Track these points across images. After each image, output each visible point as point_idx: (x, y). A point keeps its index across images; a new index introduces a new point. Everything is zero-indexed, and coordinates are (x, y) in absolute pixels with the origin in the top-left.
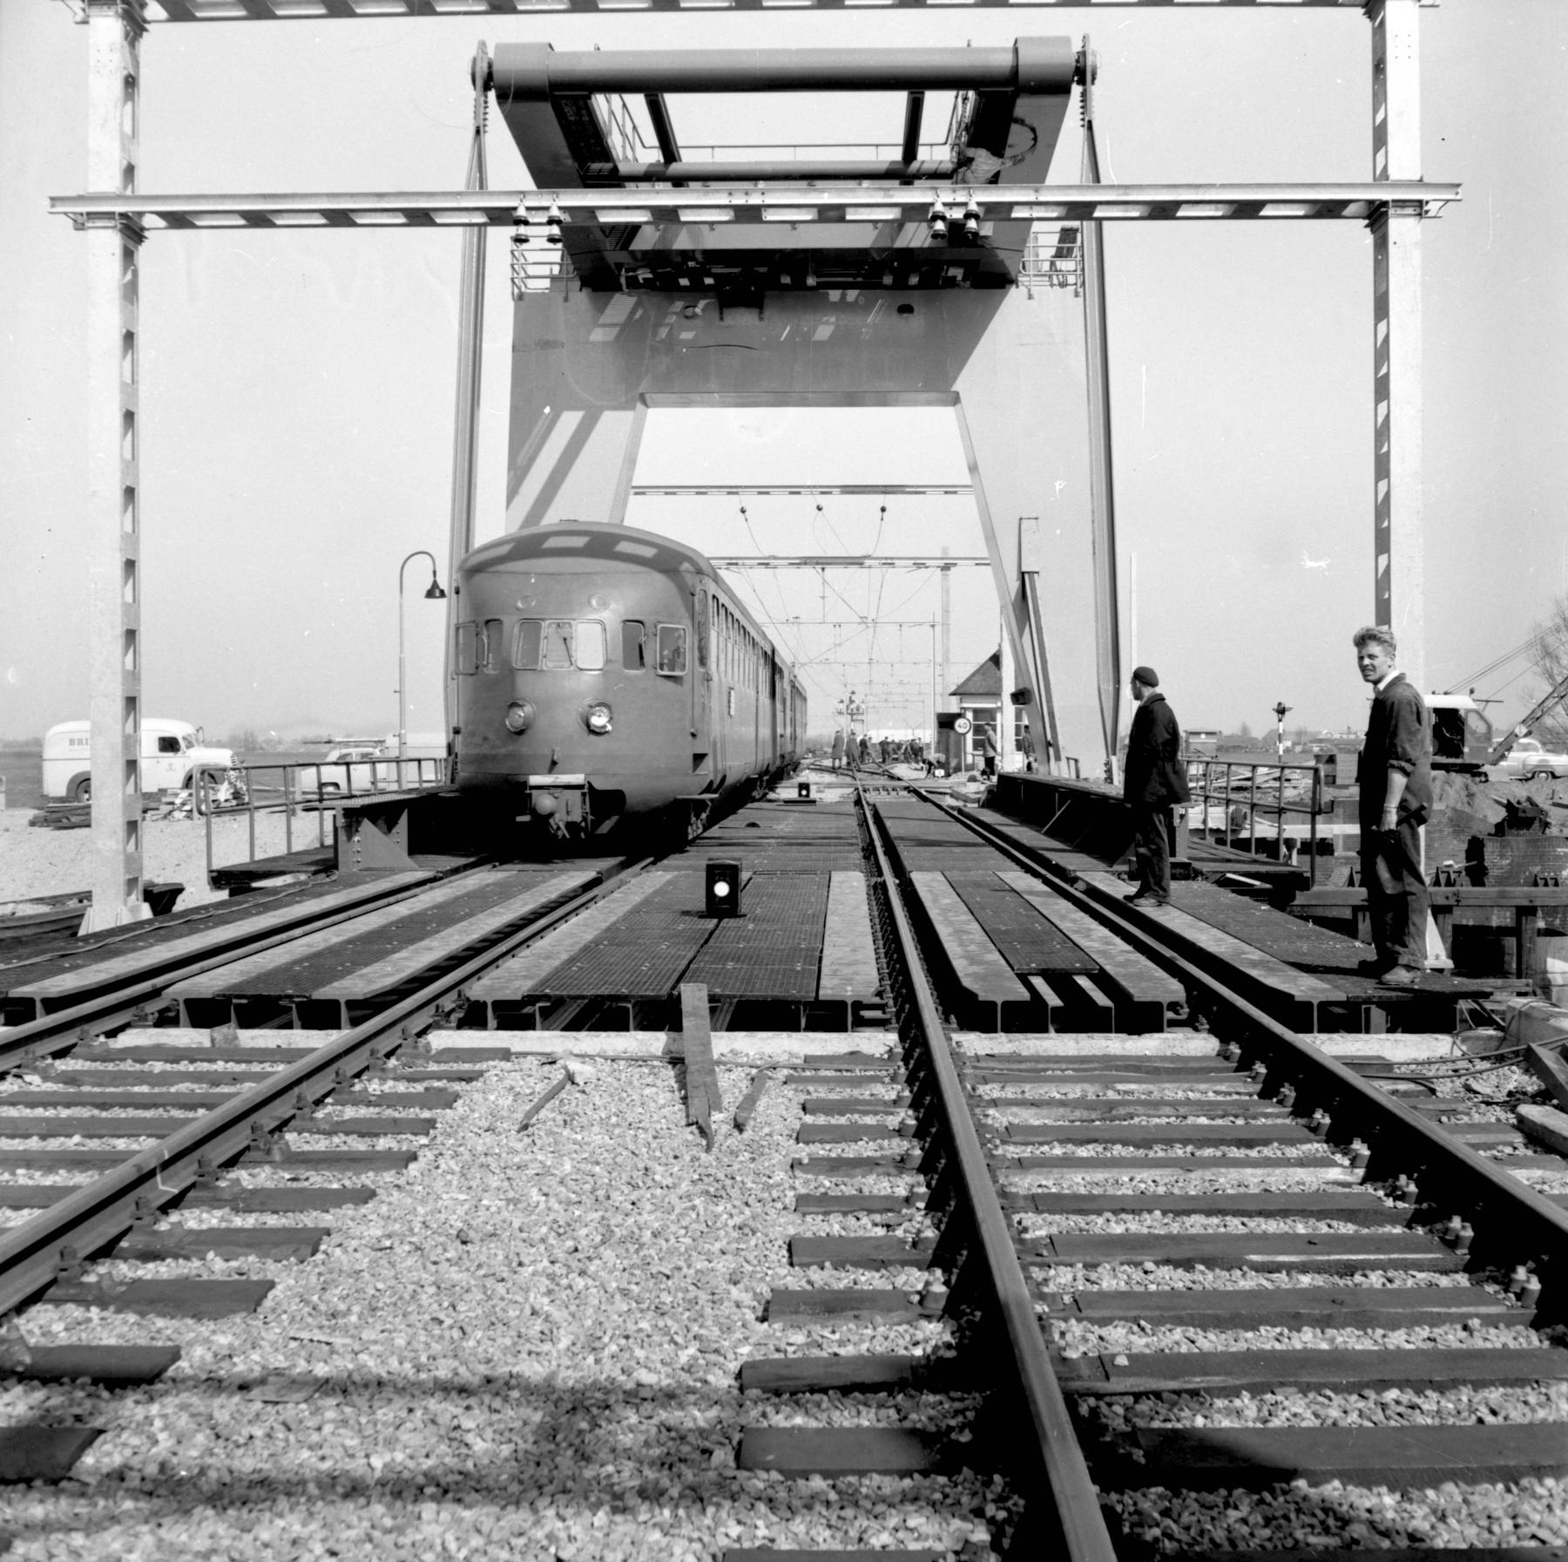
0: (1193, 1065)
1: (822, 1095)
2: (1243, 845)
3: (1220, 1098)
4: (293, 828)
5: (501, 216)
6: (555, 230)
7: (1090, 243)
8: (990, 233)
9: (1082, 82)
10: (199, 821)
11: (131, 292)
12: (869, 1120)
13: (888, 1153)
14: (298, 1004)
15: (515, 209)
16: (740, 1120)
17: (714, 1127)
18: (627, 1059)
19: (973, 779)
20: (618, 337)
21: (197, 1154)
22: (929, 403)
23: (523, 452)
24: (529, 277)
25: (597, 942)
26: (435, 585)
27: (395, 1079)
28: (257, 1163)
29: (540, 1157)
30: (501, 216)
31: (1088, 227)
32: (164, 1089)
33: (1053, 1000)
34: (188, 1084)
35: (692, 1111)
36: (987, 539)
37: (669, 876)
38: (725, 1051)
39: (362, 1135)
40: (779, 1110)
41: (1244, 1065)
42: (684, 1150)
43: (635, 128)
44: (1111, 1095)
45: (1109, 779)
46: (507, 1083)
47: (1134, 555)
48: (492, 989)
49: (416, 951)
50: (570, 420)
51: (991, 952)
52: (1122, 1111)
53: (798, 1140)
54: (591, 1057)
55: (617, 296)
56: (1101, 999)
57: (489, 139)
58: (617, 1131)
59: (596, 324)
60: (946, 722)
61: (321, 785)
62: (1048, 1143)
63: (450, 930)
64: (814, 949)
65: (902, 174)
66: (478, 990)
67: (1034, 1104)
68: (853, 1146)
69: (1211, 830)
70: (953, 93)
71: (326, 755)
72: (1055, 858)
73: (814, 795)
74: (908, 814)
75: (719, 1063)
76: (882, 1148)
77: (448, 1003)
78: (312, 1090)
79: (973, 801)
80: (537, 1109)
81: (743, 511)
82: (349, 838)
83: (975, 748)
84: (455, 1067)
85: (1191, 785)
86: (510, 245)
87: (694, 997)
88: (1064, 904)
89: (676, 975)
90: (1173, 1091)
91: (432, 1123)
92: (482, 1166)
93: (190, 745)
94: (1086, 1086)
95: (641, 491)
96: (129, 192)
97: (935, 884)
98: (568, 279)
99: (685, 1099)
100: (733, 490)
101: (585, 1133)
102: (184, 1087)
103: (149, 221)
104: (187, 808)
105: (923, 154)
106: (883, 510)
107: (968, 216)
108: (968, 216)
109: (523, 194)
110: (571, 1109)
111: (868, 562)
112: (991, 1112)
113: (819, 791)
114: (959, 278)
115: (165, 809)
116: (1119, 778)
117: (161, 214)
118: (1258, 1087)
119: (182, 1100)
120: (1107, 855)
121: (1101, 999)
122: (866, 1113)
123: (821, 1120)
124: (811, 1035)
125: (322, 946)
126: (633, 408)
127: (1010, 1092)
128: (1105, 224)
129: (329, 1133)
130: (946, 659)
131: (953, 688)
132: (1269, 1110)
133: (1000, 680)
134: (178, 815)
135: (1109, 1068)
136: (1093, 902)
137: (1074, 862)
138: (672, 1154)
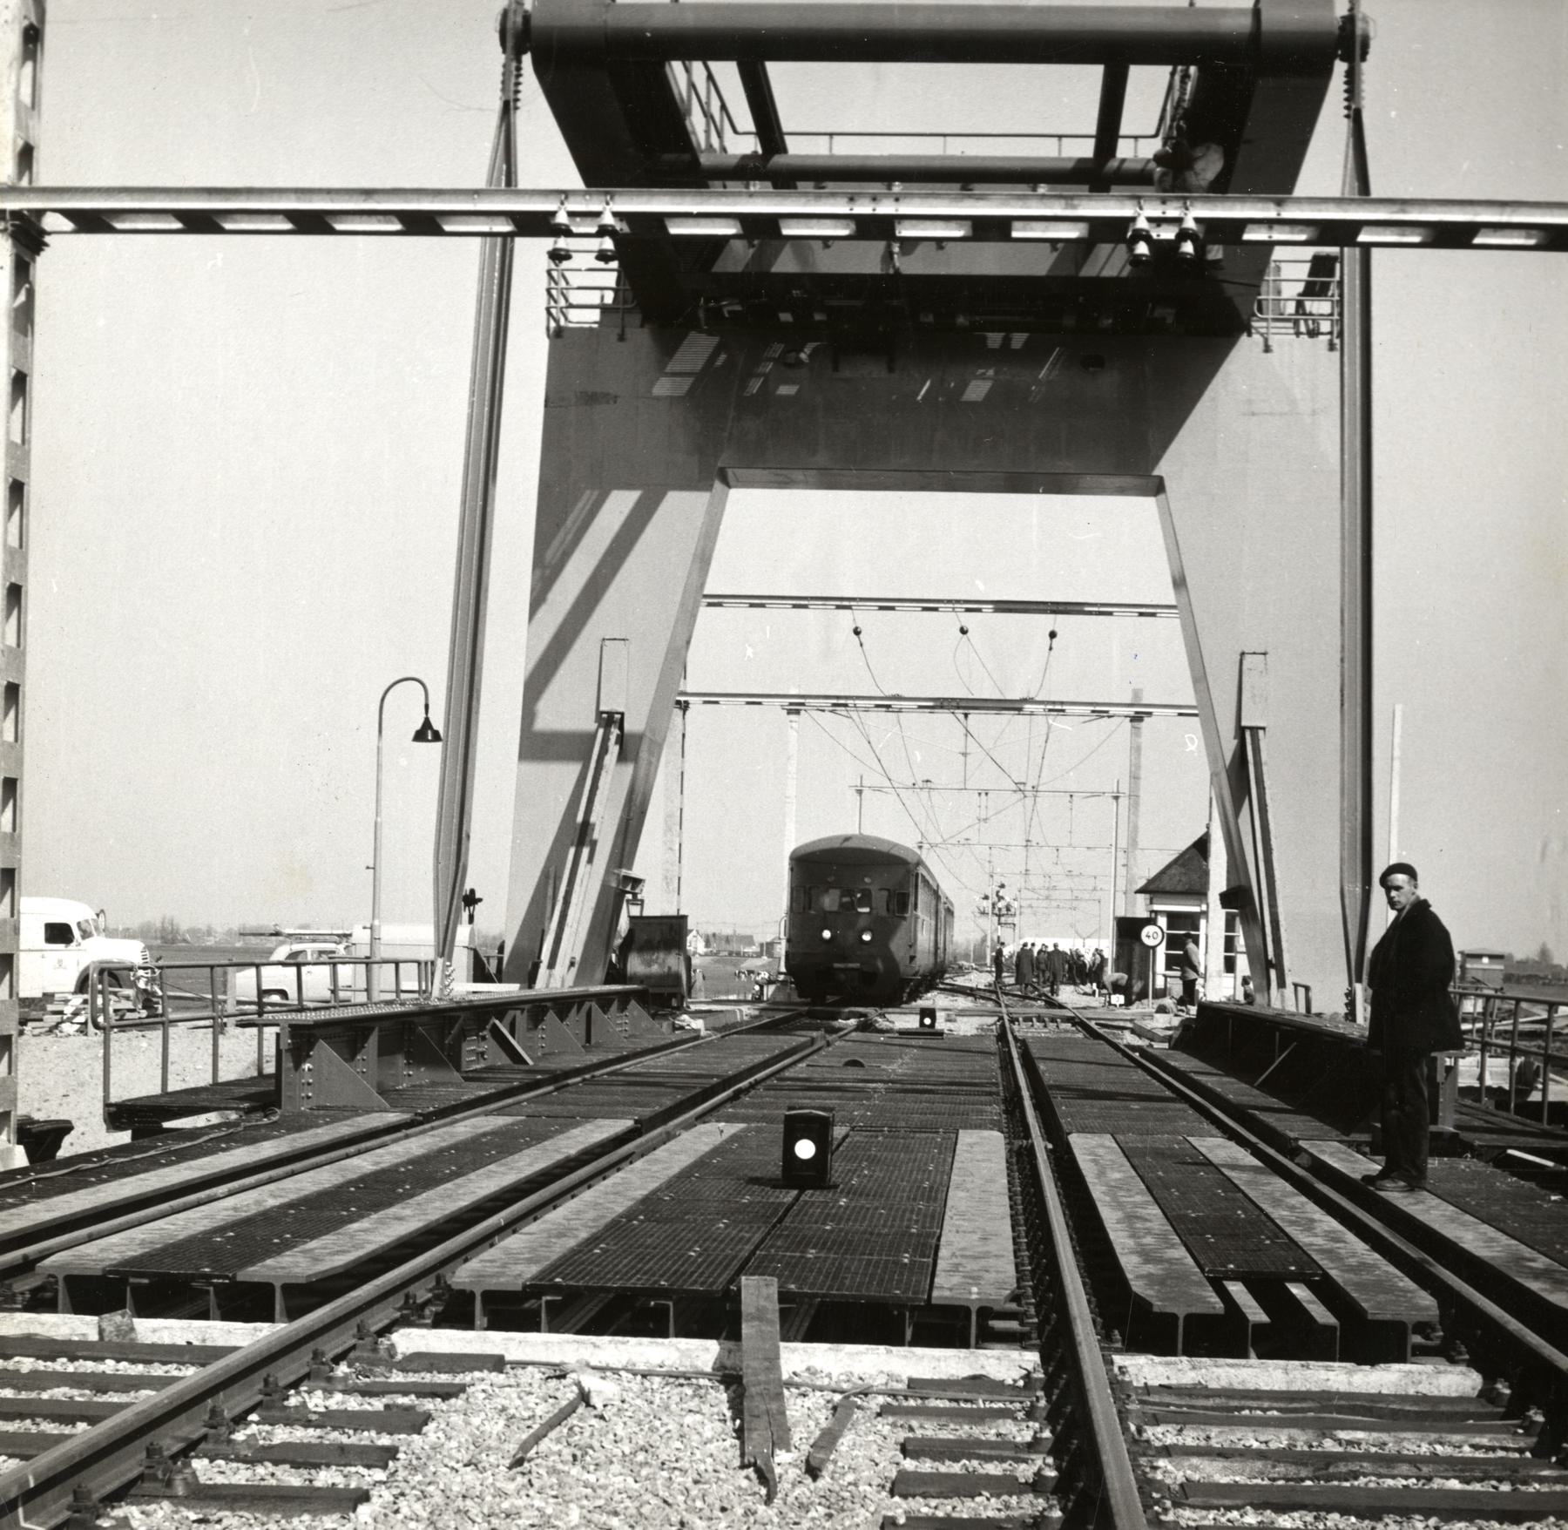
0: (1444, 1408)
1: (929, 1433)
2: (1535, 1111)
3: (1479, 1454)
4: (221, 1051)
5: (534, 224)
6: (608, 244)
7: (1352, 280)
8: (1220, 256)
9: (1348, 57)
10: (95, 1037)
11: (24, 319)
12: (993, 1469)
13: (1016, 1514)
14: (216, 1286)
15: (553, 214)
16: (813, 1463)
17: (778, 1470)
18: (664, 1375)
19: (1162, 1010)
20: (691, 392)
21: (72, 1483)
22: (1122, 491)
23: (556, 543)
24: (571, 306)
25: (630, 1215)
26: (427, 724)
27: (344, 1392)
28: (154, 1498)
29: (538, 1503)
30: (534, 224)
31: (1351, 255)
32: (33, 1395)
33: (1256, 1313)
34: (65, 1390)
35: (749, 1448)
36: (1195, 681)
37: (731, 1129)
38: (800, 1369)
39: (296, 1465)
40: (869, 1451)
41: (1515, 1410)
42: (735, 1500)
43: (723, 107)
44: (1329, 1445)
45: (1351, 1015)
46: (499, 1402)
47: (1399, 708)
48: (480, 1276)
49: (381, 1222)
50: (620, 504)
51: (1173, 1246)
52: (1343, 1468)
53: (892, 1493)
54: (615, 1371)
55: (693, 335)
56: (1321, 1314)
57: (521, 119)
58: (644, 1472)
59: (661, 371)
60: (1128, 929)
61: (262, 993)
62: (1238, 1508)
63: (430, 1194)
64: (930, 1235)
65: (1097, 174)
66: (463, 1275)
67: (1223, 1454)
68: (969, 1503)
69: (1489, 1089)
70: (1169, 68)
71: (270, 952)
72: (1270, 1119)
73: (941, 1025)
74: (1070, 1054)
75: (789, 1384)
76: (1007, 1507)
77: (422, 1293)
78: (230, 1404)
79: (1163, 1040)
80: (537, 1438)
81: (857, 632)
82: (297, 1066)
83: (1168, 967)
84: (428, 1377)
85: (1465, 1027)
86: (546, 263)
87: (759, 1294)
88: (1280, 1185)
89: (736, 1264)
90: (1416, 1444)
91: (392, 1452)
92: (458, 1511)
93: (86, 934)
94: (1295, 1432)
95: (717, 601)
96: (24, 183)
97: (1101, 1151)
98: (630, 311)
99: (740, 1433)
100: (844, 603)
101: (601, 1474)
102: (60, 1393)
103: (51, 222)
104: (81, 1019)
105: (1124, 150)
106: (1053, 635)
107: (1184, 235)
108: (1184, 235)
109: (566, 194)
110: (584, 1440)
111: (1028, 707)
112: (1162, 1463)
113: (949, 1020)
114: (1170, 320)
115: (51, 1020)
116: (1363, 1013)
117: (67, 213)
118: (1532, 1441)
119: (57, 1411)
120: (1342, 1121)
121: (1321, 1314)
122: (988, 1459)
123: (927, 1466)
124: (919, 1350)
125: (253, 1210)
126: (709, 488)
127: (1190, 1437)
128: (1375, 252)
129: (251, 1462)
130: (1133, 842)
131: (1141, 883)
132: (1545, 1473)
133: (1206, 873)
134: (66, 1027)
135: (1329, 1409)
136: (1317, 1182)
137: (1293, 1126)
138: (718, 1505)
